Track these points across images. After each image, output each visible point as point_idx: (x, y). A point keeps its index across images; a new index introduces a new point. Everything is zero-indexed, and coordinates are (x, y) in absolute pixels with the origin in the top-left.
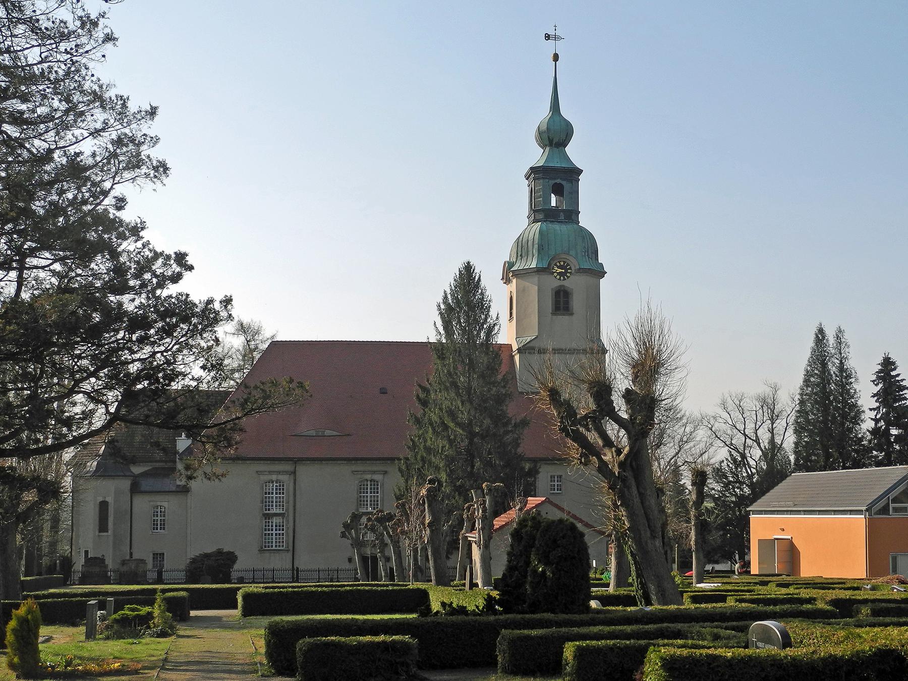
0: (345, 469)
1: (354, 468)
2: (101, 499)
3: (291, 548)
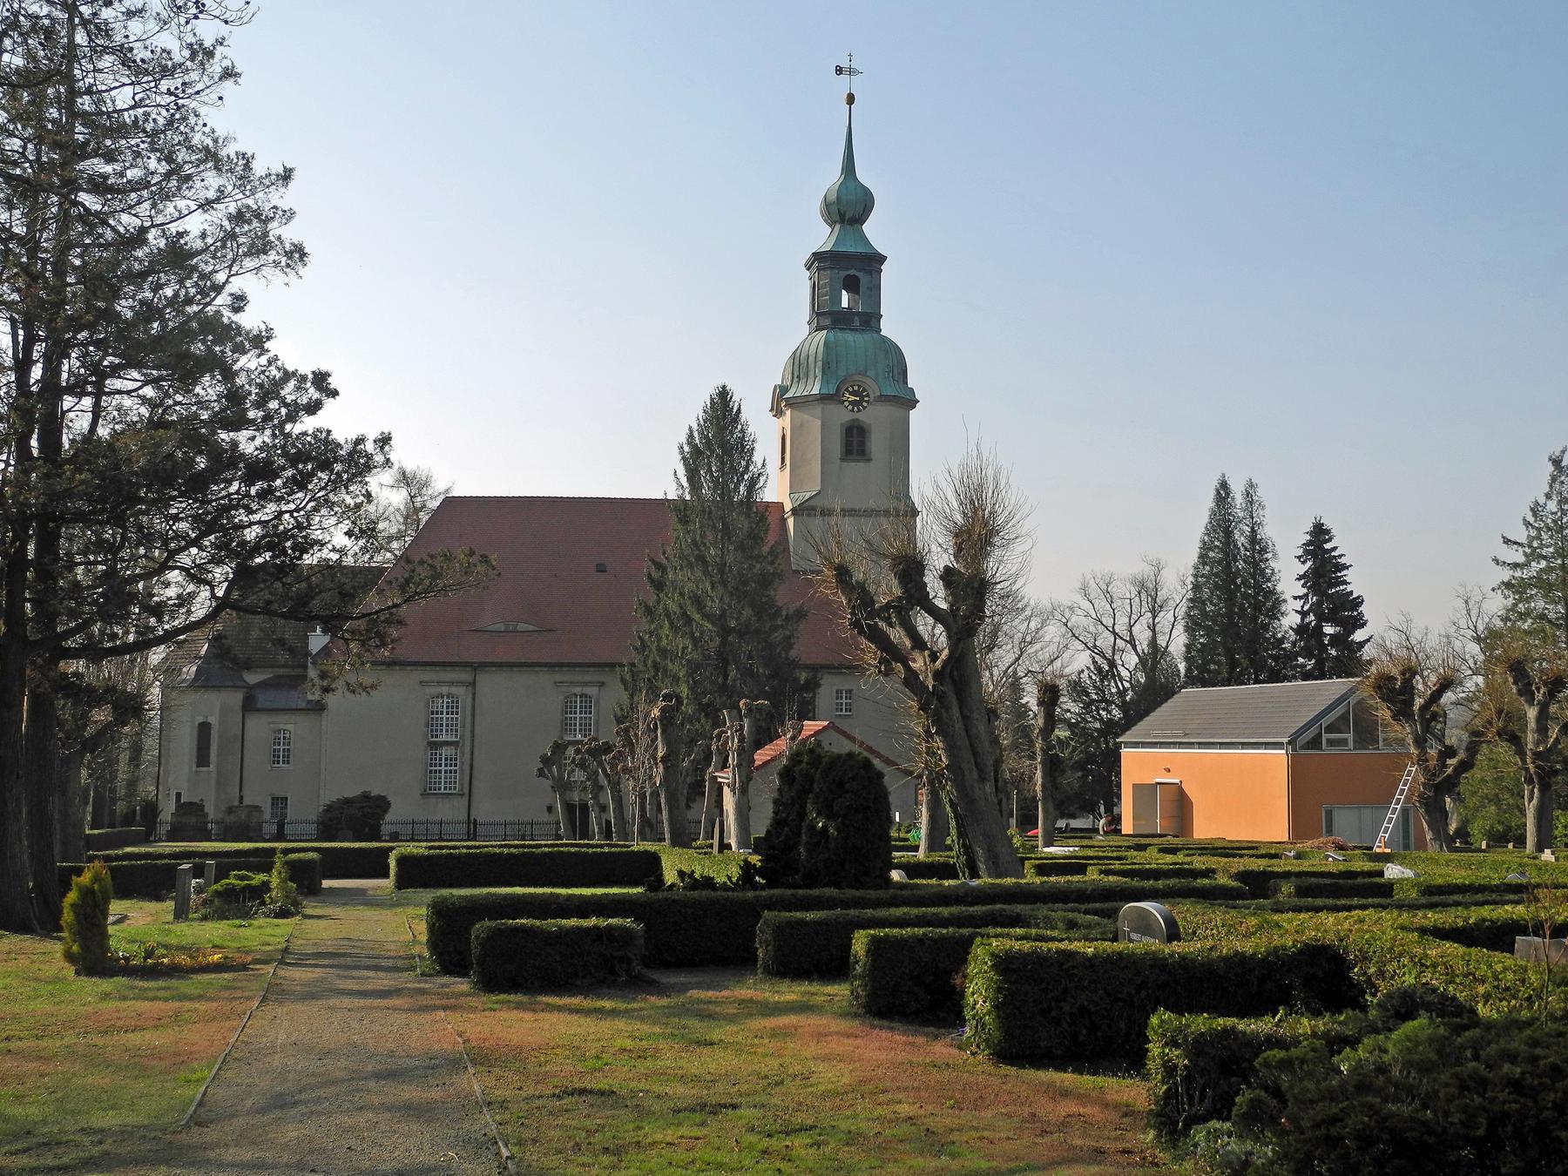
0: (546, 679)
1: (557, 677)
2: (200, 719)
3: (466, 791)
